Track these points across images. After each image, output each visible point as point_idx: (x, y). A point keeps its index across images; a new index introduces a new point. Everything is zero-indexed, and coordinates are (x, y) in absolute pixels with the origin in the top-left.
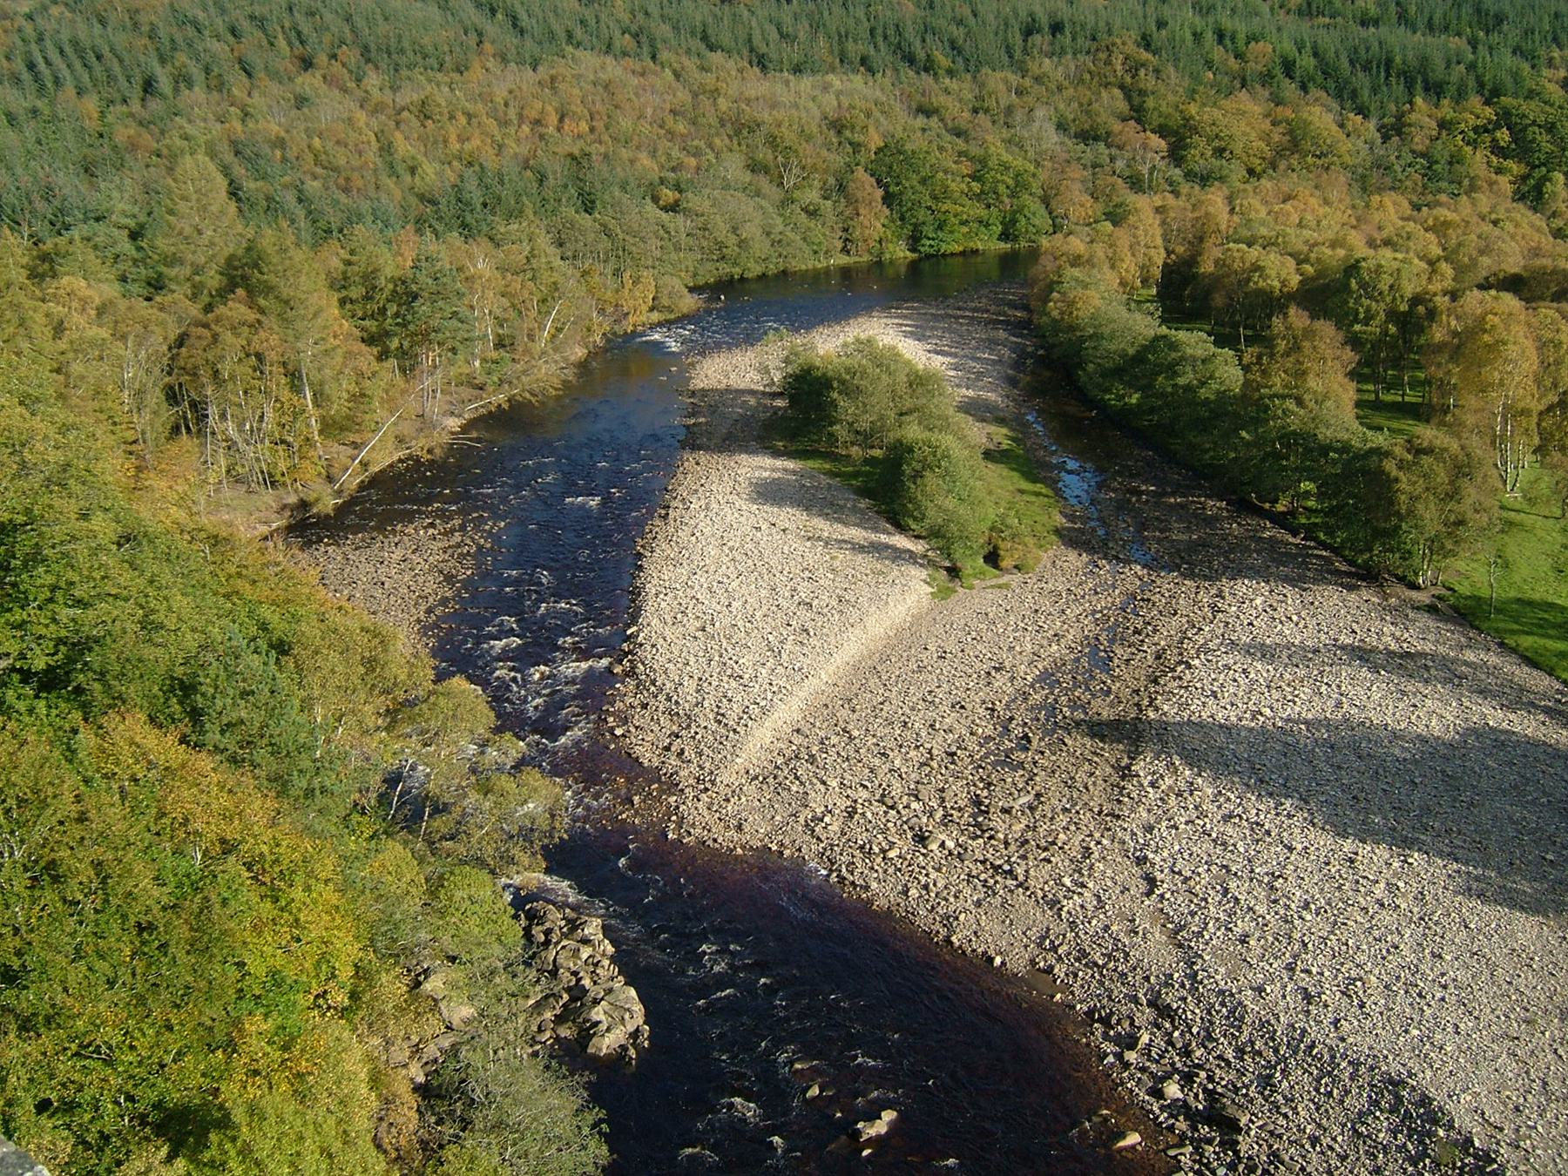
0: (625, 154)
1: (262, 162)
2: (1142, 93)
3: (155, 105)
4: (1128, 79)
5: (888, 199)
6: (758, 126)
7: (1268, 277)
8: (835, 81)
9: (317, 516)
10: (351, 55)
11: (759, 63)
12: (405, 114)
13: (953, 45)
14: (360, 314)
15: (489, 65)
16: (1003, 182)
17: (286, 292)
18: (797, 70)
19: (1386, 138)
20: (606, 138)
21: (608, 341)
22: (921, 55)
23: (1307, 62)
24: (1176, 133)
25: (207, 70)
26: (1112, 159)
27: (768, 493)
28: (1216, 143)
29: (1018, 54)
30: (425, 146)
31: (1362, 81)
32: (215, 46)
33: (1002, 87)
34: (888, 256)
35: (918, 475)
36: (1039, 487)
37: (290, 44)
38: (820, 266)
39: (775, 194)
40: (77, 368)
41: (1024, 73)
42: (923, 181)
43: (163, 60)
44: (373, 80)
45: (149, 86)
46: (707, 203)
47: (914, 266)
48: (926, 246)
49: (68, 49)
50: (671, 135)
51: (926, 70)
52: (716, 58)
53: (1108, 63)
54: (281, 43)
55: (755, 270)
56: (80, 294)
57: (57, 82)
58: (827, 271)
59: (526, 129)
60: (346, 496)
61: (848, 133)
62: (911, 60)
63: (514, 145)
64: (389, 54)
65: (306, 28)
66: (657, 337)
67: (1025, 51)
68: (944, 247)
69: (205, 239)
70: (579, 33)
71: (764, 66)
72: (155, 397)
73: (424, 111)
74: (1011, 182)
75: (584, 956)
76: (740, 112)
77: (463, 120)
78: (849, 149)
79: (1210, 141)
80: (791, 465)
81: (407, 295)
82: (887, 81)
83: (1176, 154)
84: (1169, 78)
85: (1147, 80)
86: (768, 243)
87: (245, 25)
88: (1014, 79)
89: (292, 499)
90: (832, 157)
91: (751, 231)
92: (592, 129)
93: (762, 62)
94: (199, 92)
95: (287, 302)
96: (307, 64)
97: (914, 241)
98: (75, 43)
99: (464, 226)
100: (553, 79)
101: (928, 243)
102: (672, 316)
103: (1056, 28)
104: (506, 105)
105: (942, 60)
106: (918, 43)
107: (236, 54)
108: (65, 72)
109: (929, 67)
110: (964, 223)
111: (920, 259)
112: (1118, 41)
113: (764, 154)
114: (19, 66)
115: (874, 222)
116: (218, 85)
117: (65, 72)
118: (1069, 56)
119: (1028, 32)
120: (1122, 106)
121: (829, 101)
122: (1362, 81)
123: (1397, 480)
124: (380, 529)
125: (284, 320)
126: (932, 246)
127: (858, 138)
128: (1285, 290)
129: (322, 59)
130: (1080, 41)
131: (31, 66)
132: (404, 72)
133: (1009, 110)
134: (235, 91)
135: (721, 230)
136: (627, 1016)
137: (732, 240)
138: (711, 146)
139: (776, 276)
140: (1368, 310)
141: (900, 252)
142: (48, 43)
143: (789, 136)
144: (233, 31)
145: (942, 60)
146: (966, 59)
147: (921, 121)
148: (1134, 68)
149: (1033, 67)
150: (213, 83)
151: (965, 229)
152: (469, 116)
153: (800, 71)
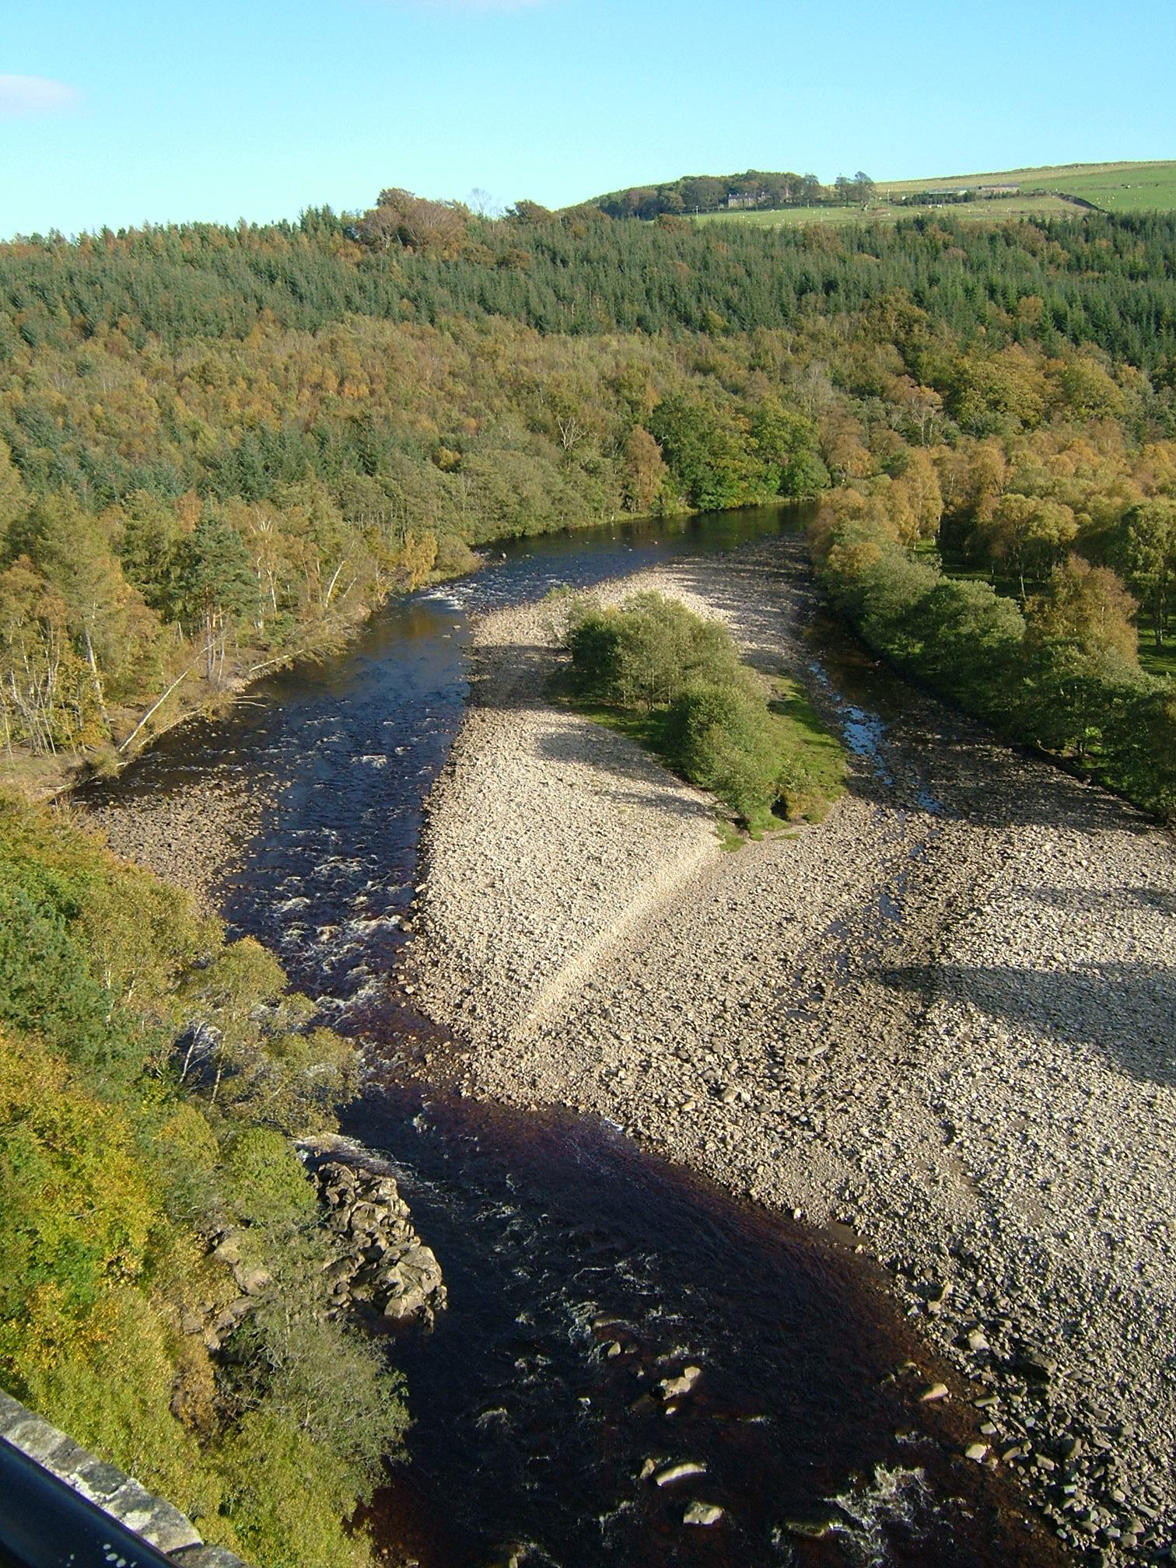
2: (916, 348)
4: (902, 336)
5: (667, 456)
6: (537, 386)
9: (103, 778)
10: (131, 322)
14: (144, 577)
16: (781, 437)
17: (71, 557)
18: (575, 331)
19: (1158, 388)
20: (386, 400)
22: (697, 315)
23: (1078, 315)
24: (950, 387)
28: (991, 396)
29: (792, 313)
31: (1133, 334)
33: (778, 345)
34: (668, 512)
35: (704, 728)
38: (600, 523)
42: (702, 438)
47: (694, 521)
50: (451, 396)
51: (702, 329)
52: (495, 320)
53: (882, 319)
54: (63, 312)
55: (536, 527)
60: (131, 758)
62: (687, 320)
64: (169, 321)
66: (439, 595)
67: (799, 309)
68: (723, 502)
70: (357, 298)
71: (541, 327)
73: (205, 377)
75: (380, 1217)
78: (628, 407)
79: (984, 393)
81: (190, 558)
82: (664, 340)
83: (951, 407)
89: (77, 762)
90: (610, 415)
91: (532, 489)
92: (372, 392)
93: (540, 324)
95: (70, 567)
96: (88, 332)
97: (694, 497)
99: (246, 489)
100: (333, 343)
101: (708, 498)
102: (455, 575)
104: (286, 369)
105: (717, 319)
106: (693, 303)
109: (704, 326)
110: (743, 478)
111: (700, 515)
112: (892, 298)
113: (543, 414)
119: (802, 291)
120: (897, 361)
121: (607, 362)
122: (1133, 334)
125: (68, 585)
127: (635, 396)
128: (1064, 538)
129: (103, 327)
132: (185, 339)
133: (786, 367)
135: (502, 488)
136: (424, 1277)
140: (1147, 557)
141: (679, 508)
143: (568, 396)
145: (717, 319)
147: (698, 379)
148: (908, 325)
149: (808, 324)
151: (744, 484)
152: (250, 382)
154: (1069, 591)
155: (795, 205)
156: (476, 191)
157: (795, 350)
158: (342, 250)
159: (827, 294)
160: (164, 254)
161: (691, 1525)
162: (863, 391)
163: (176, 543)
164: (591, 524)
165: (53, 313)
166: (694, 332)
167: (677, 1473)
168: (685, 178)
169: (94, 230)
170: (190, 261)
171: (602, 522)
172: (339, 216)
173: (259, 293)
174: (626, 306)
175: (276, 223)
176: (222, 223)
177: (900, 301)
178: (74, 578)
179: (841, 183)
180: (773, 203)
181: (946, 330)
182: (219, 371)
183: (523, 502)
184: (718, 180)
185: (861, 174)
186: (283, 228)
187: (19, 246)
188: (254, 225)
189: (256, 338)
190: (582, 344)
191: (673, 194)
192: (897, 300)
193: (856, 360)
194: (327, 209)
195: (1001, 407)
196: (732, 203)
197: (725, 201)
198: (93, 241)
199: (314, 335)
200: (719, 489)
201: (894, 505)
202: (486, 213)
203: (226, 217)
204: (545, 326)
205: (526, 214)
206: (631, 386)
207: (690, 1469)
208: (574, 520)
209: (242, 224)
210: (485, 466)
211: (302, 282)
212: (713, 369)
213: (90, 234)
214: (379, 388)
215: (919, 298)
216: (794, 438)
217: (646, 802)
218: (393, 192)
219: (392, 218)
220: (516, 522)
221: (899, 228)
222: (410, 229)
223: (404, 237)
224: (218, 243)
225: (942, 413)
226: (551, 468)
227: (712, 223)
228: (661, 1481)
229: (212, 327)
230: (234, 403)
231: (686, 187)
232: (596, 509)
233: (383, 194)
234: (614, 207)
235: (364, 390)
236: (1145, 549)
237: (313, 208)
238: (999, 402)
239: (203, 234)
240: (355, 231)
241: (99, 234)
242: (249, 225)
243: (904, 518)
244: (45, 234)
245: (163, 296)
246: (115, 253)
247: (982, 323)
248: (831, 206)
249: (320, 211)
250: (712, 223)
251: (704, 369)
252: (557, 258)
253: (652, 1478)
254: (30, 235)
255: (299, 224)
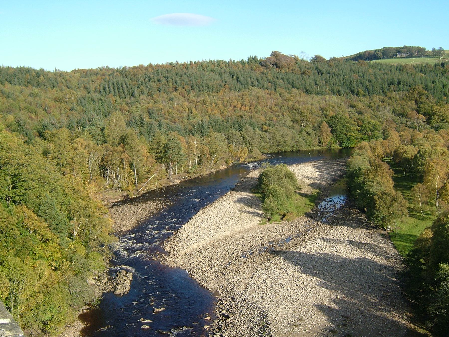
0: (257, 115)
1: (153, 114)
2: (421, 103)
3: (133, 99)
4: (418, 98)
5: (332, 131)
6: (298, 109)
7: (408, 154)
8: (327, 97)
9: (131, 199)
10: (188, 87)
11: (306, 92)
12: (199, 103)
13: (366, 88)
14: (156, 152)
15: (226, 91)
16: (369, 127)
17: (132, 145)
18: (317, 94)
20: (253, 111)
21: (234, 165)
24: (429, 115)
25: (149, 90)
26: (407, 122)
27: (240, 201)
28: (441, 118)
29: (386, 91)
30: (201, 112)
32: (152, 84)
33: (378, 100)
34: (332, 147)
36: (312, 204)
37: (173, 84)
38: (310, 149)
39: (299, 128)
40: (75, 158)
41: (386, 96)
42: (344, 126)
43: (138, 87)
44: (192, 94)
45: (133, 94)
46: (275, 130)
47: (341, 150)
48: (344, 145)
49: (115, 84)
50: (272, 111)
51: (357, 95)
52: (294, 90)
53: (412, 94)
54: (170, 84)
55: (289, 149)
56: (81, 142)
57: (110, 92)
58: (313, 150)
59: (231, 108)
60: (140, 195)
61: (325, 112)
62: (353, 92)
63: (226, 112)
64: (199, 87)
65: (178, 80)
67: (388, 90)
68: (350, 145)
69: (116, 131)
70: (255, 82)
71: (308, 93)
72: (97, 168)
73: (204, 103)
74: (372, 128)
75: (124, 279)
76: (294, 105)
77: (214, 105)
78: (324, 116)
79: (439, 117)
80: (252, 195)
81: (166, 148)
82: (344, 98)
83: (428, 121)
84: (430, 98)
85: (424, 98)
86: (293, 142)
87: (163, 79)
88: (382, 98)
89: (125, 194)
90: (317, 118)
91: (289, 138)
92: (250, 109)
93: (307, 92)
94: (144, 97)
95: (131, 147)
96: (176, 89)
98: (117, 83)
99: (201, 133)
100: (243, 95)
101: (345, 144)
102: (256, 160)
103: (399, 83)
104: (227, 101)
106: (356, 87)
107: (158, 86)
108: (112, 90)
110: (357, 139)
111: (343, 149)
112: (417, 87)
113: (298, 117)
114: (101, 88)
115: (328, 138)
116: (150, 94)
117: (112, 90)
118: (401, 92)
120: (414, 106)
121: (323, 104)
123: (377, 201)
124: (143, 202)
126: (346, 145)
129: (180, 88)
130: (405, 87)
131: (104, 88)
132: (202, 92)
133: (378, 107)
134: (154, 96)
135: (279, 138)
136: (124, 288)
137: (282, 140)
138: (283, 115)
139: (296, 152)
140: (422, 163)
141: (337, 146)
142: (110, 83)
143: (306, 112)
144: (159, 81)
145: (362, 92)
146: (369, 92)
147: (350, 109)
148: (420, 95)
149: (389, 94)
150: (150, 94)
151: (357, 141)
152: (216, 104)
153: (318, 94)
154: (374, 168)
155: (418, 57)
156: (302, 52)
157: (383, 102)
158: (257, 69)
159: (398, 86)
160: (205, 68)
161: (143, 328)
162: (401, 115)
163: (164, 144)
164: (307, 149)
165: (168, 84)
166: (354, 95)
167: (146, 321)
168: (384, 48)
169: (187, 61)
170: (213, 71)
171: (311, 148)
172: (259, 59)
173: (226, 80)
174: (335, 87)
175: (240, 60)
176: (224, 60)
177: (420, 88)
178: (132, 150)
179: (434, 50)
180: (411, 56)
181: (432, 98)
182: (208, 101)
183: (285, 142)
184: (394, 49)
185: (440, 48)
186: (242, 62)
187: (167, 65)
188: (234, 61)
189: (221, 92)
190: (317, 98)
191: (379, 53)
192: (418, 88)
193: (401, 106)
194: (256, 57)
195: (445, 121)
196: (398, 56)
197: (396, 55)
198: (187, 65)
199: (239, 92)
200: (349, 142)
201: (376, 147)
202: (305, 59)
203: (226, 58)
204: (309, 92)
205: (317, 59)
206: (327, 110)
207: (149, 321)
208: (301, 148)
209: (231, 60)
210: (274, 130)
211: (241, 77)
212: (355, 107)
213: (186, 62)
214: (252, 108)
215: (426, 88)
216: (374, 128)
217: (250, 213)
218: (275, 52)
219: (274, 59)
220: (282, 147)
221: (435, 65)
222: (278, 63)
223: (276, 65)
224: (222, 65)
225: (426, 122)
226: (295, 133)
227: (375, 63)
228: (142, 322)
229: (210, 89)
230: (210, 110)
231: (383, 51)
232: (309, 145)
233: (273, 52)
234: (359, 57)
235: (248, 108)
236: (421, 160)
237: (252, 56)
238: (444, 120)
239: (218, 63)
240: (263, 64)
241: (189, 62)
242: (232, 61)
243: (379, 151)
244: (174, 62)
245: (199, 80)
246: (192, 68)
247: (445, 96)
248: (430, 57)
249: (254, 57)
250: (375, 63)
251: (353, 107)
252: (320, 72)
253: (141, 321)
254: (170, 62)
255: (247, 61)
